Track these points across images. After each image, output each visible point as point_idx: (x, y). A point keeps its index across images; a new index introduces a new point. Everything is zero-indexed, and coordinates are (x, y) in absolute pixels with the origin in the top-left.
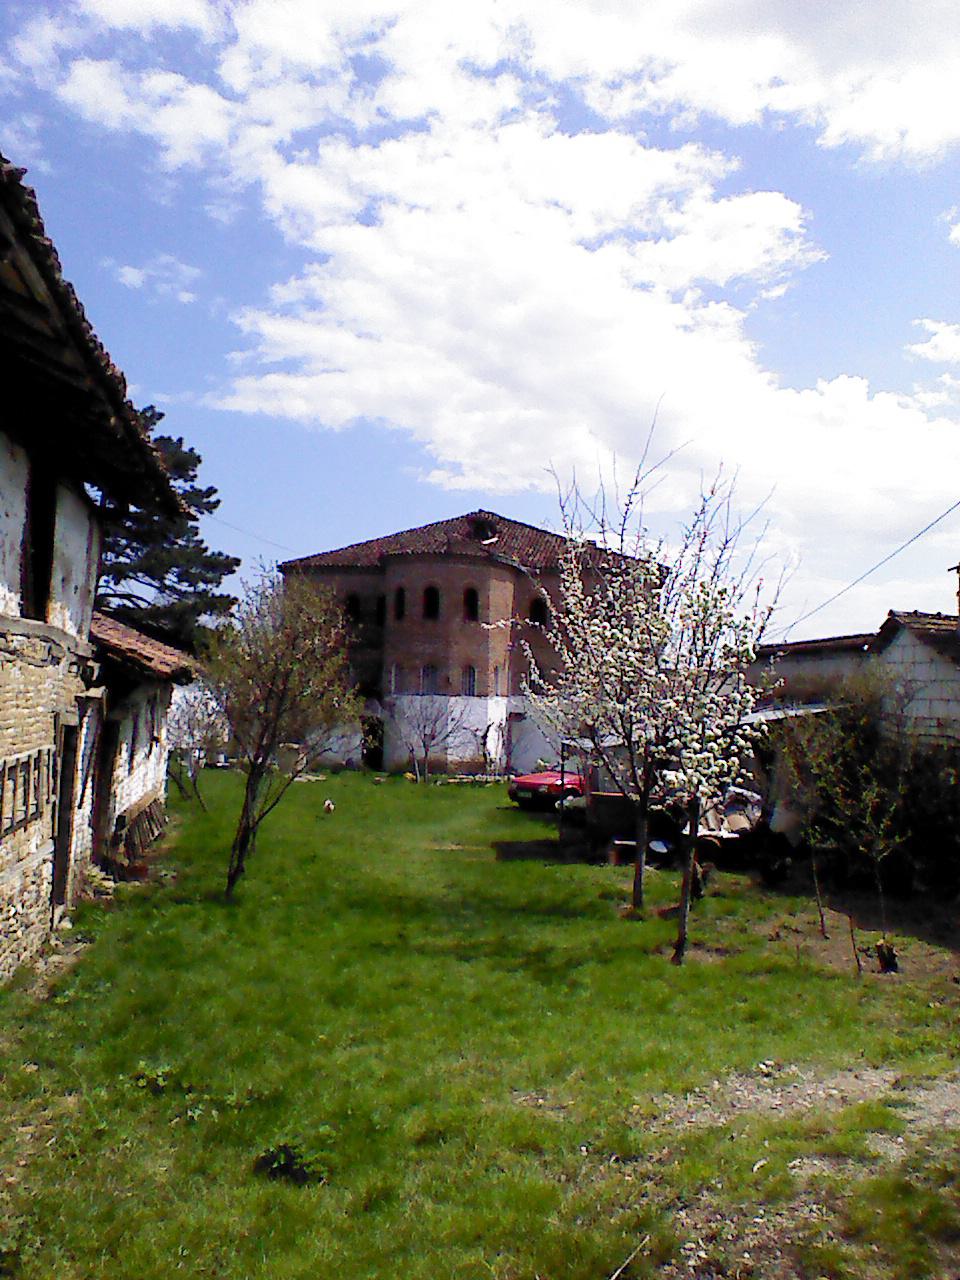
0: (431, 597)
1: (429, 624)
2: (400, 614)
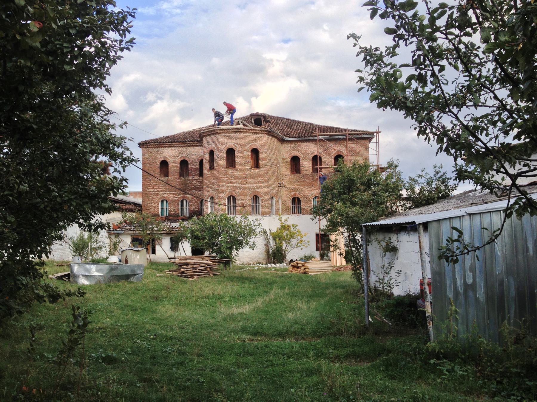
0: (231, 153)
1: (230, 170)
2: (212, 167)
